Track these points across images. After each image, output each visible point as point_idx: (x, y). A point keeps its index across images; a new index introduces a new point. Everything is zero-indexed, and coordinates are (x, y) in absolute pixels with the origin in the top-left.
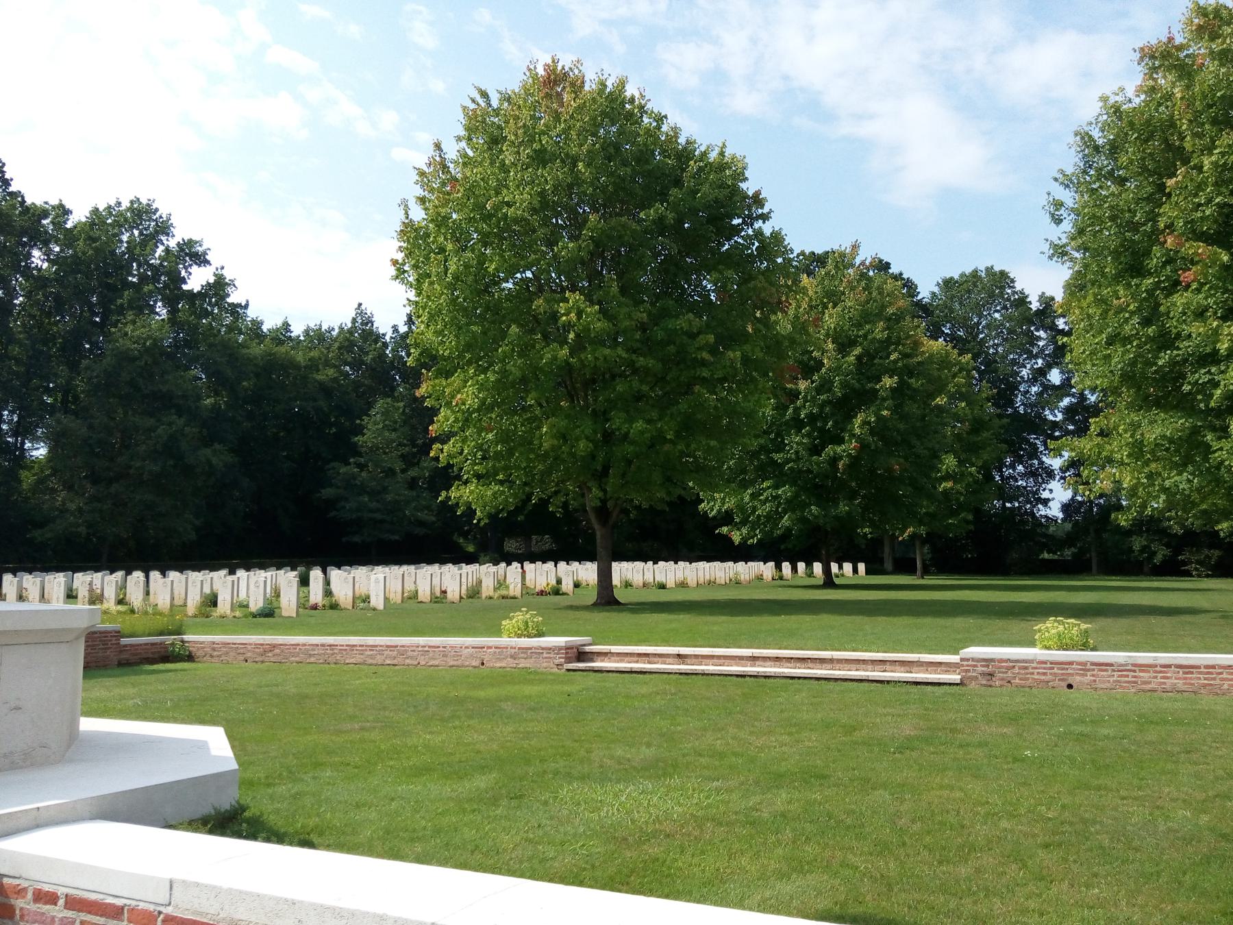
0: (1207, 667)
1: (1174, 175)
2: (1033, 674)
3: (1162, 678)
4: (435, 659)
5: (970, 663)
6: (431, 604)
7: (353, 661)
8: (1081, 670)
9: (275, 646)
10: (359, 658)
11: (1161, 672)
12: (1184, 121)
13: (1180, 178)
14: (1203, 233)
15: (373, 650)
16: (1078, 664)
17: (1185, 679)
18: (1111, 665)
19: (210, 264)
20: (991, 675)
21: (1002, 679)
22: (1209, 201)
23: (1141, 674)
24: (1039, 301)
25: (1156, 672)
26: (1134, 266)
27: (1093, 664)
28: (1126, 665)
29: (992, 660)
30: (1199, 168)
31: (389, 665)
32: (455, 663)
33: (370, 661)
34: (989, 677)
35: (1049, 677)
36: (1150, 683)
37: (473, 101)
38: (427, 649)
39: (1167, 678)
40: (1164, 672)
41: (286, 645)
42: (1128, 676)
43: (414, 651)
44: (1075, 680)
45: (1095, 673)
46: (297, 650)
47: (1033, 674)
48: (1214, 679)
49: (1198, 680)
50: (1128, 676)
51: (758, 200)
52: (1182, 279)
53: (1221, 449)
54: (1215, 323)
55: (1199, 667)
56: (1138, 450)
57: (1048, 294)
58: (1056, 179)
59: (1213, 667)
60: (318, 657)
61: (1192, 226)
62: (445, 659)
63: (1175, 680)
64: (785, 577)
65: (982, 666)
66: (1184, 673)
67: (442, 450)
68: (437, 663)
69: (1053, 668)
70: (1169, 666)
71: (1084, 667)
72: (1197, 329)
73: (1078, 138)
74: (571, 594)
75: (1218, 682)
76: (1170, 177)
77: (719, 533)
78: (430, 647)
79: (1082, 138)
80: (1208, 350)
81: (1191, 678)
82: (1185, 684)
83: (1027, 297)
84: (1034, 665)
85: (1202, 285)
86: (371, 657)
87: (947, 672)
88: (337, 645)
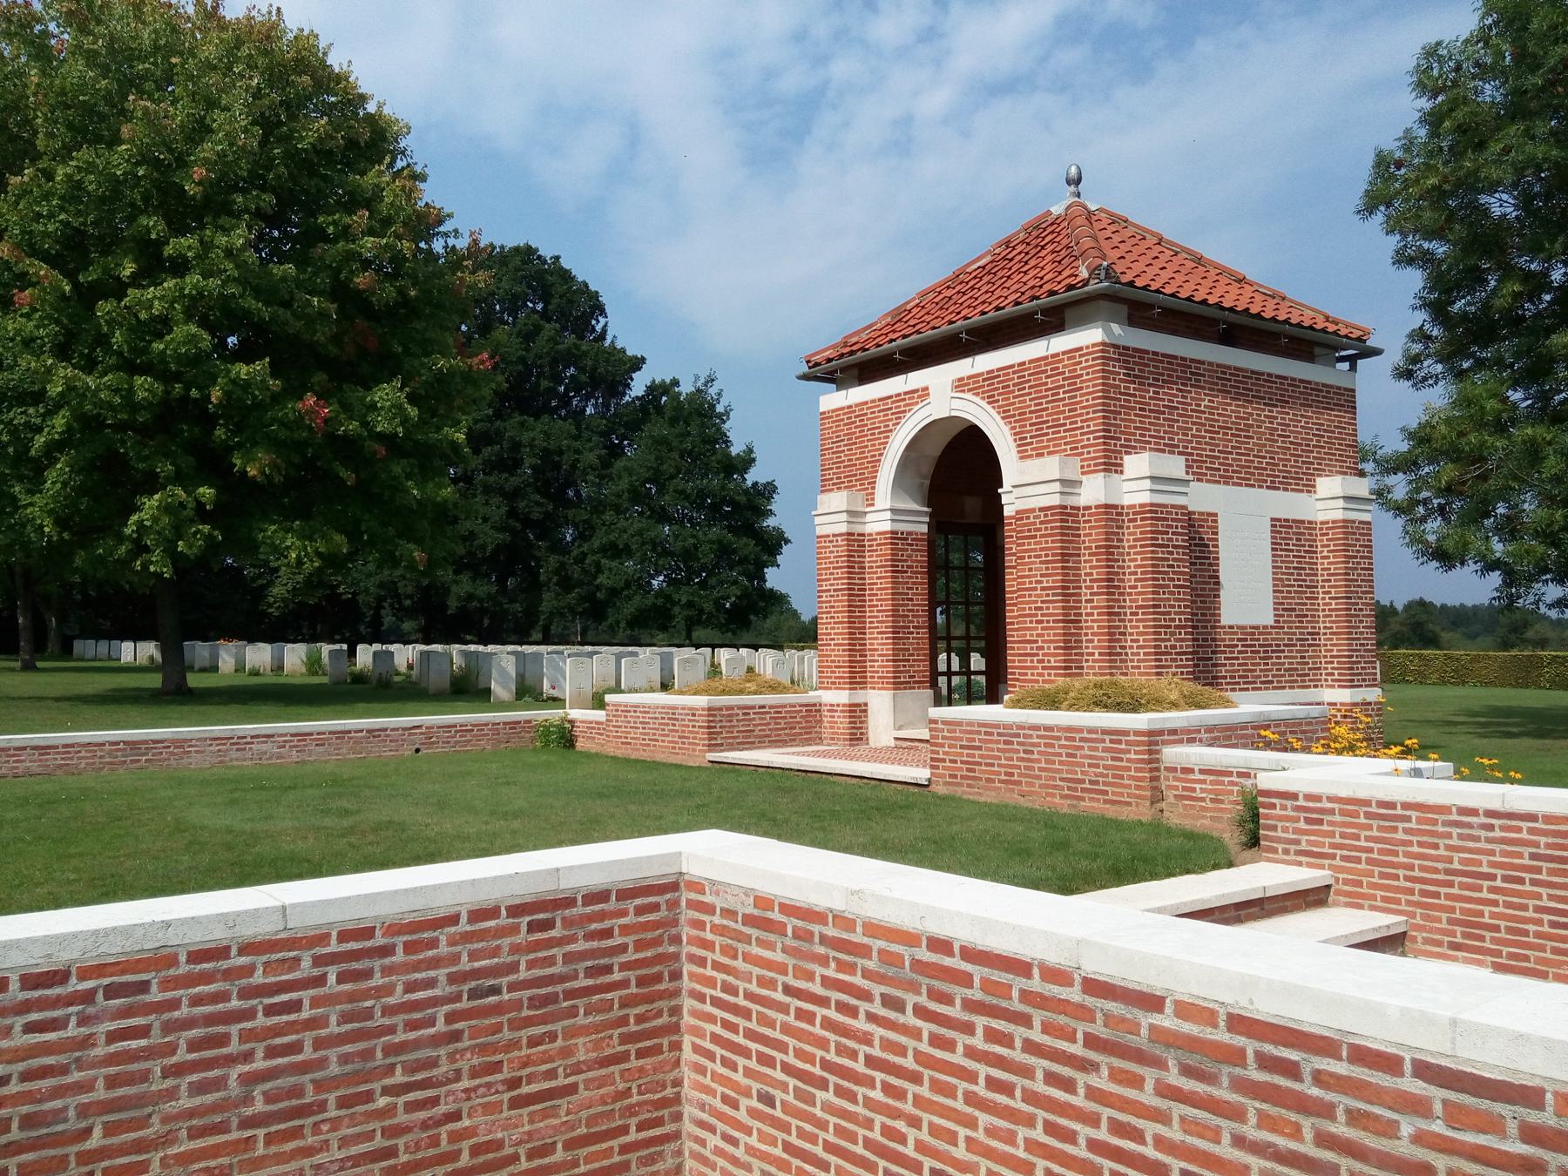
1: (20, 173)
3: (14, 762)
11: (14, 755)
12: (39, 114)
13: (26, 179)
17: (41, 760)
19: (1403, 430)
22: (51, 216)
30: (49, 175)
39: (21, 761)
48: (72, 759)
49: (54, 760)
52: (16, 299)
53: (31, 504)
54: (50, 362)
59: (72, 746)
61: (30, 239)
63: (30, 763)
66: (40, 754)
70: (25, 748)
72: (27, 362)
75: (75, 761)
76: (16, 175)
80: (36, 388)
81: (46, 760)
85: (35, 310)
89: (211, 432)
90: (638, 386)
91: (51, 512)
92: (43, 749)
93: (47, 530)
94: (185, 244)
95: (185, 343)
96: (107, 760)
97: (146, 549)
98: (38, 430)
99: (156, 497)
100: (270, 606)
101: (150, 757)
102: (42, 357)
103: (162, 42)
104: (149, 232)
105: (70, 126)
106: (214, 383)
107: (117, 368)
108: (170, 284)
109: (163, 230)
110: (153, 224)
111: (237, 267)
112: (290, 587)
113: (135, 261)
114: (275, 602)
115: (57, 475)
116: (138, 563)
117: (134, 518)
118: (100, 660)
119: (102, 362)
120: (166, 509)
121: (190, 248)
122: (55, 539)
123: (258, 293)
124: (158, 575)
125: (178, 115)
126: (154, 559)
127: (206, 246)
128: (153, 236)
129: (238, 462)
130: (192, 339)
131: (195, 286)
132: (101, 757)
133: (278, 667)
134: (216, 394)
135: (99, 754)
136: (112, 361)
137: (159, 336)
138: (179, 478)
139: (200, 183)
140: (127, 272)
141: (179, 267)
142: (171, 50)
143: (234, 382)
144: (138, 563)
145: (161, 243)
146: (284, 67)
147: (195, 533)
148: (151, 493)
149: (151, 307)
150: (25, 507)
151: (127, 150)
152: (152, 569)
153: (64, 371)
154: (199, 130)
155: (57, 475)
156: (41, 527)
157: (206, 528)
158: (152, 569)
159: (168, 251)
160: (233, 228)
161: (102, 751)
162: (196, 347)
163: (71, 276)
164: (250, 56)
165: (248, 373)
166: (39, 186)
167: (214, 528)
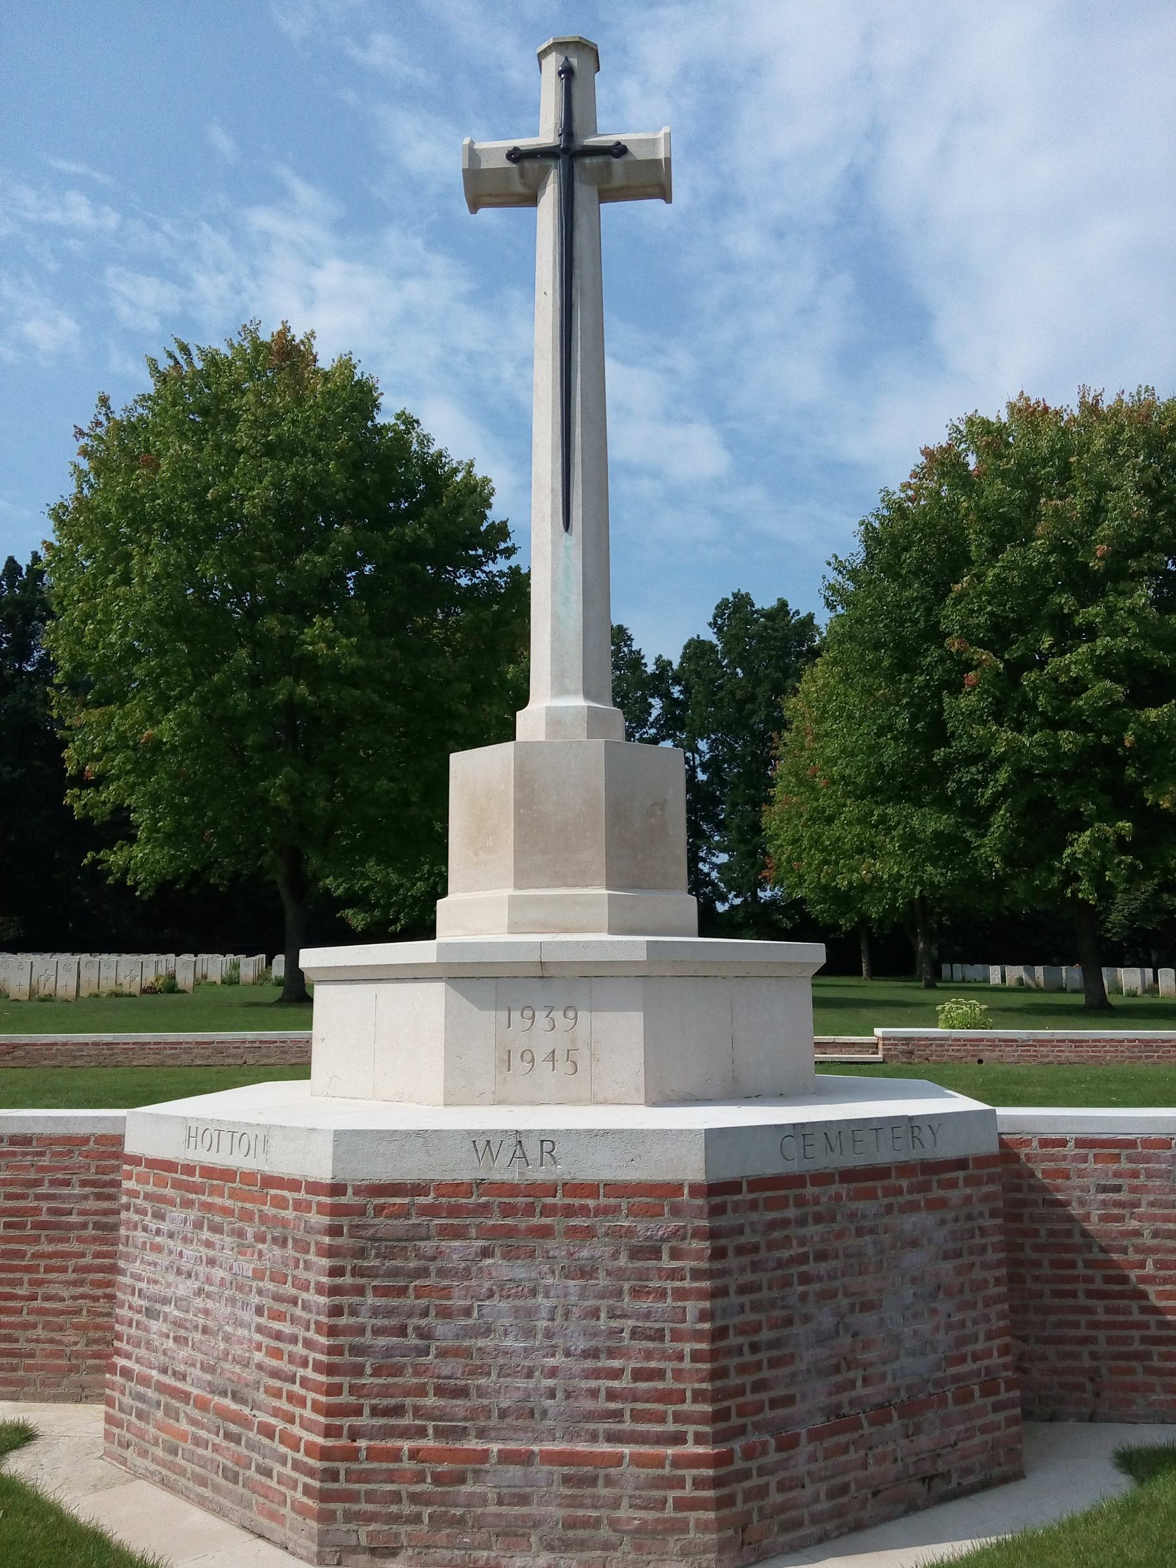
0: (1094, 1041)
2: (948, 1050)
4: (269, 1057)
5: (892, 1042)
6: (30, 1003)
7: (142, 1062)
8: (990, 1046)
9: (15, 1047)
10: (152, 1060)
11: (1056, 1046)
14: (978, 639)
15: (176, 1049)
16: (988, 1040)
17: (1077, 1052)
18: (1016, 1041)
20: (911, 1053)
21: (921, 1057)
22: (980, 609)
23: (1041, 1049)
24: (656, 664)
25: (1052, 1046)
26: (906, 661)
27: (1000, 1040)
28: (1029, 1041)
29: (911, 1039)
31: (200, 1066)
32: (298, 1060)
33: (171, 1062)
34: (909, 1055)
35: (962, 1054)
36: (1048, 1056)
37: (171, 355)
38: (257, 1045)
39: (1063, 1051)
40: (1059, 1046)
41: (35, 1045)
42: (1030, 1051)
43: (239, 1048)
44: (985, 1056)
45: (1002, 1048)
46: (54, 1051)
47: (948, 1050)
48: (1100, 1051)
49: (1086, 1052)
50: (1030, 1051)
51: (501, 531)
55: (1087, 1041)
56: (910, 839)
57: (665, 658)
58: (829, 564)
60: (88, 1059)
61: (968, 631)
62: (284, 1056)
63: (1068, 1054)
64: (181, 985)
65: (902, 1044)
66: (1076, 1047)
67: (79, 797)
68: (272, 1062)
69: (966, 1045)
70: (1064, 1041)
71: (993, 1043)
72: (978, 731)
73: (863, 527)
74: (191, 992)
77: (341, 916)
78: (261, 1042)
79: (867, 528)
82: (1076, 1056)
83: (643, 658)
84: (949, 1043)
86: (173, 1057)
87: (860, 1052)
88: (119, 1044)
89: (1123, 771)
90: (709, 635)
91: (998, 851)
92: (1078, 1042)
93: (997, 866)
94: (1094, 612)
95: (1100, 698)
96: (1127, 1054)
97: (1077, 879)
98: (984, 784)
99: (1088, 833)
100: (1108, 931)
101: (1160, 1054)
102: (988, 725)
103: (1058, 447)
104: (1062, 608)
105: (992, 535)
106: (1126, 729)
107: (1041, 727)
108: (1084, 648)
109: (1074, 605)
110: (1065, 601)
111: (1139, 624)
112: (1126, 912)
113: (1051, 634)
114: (1113, 928)
115: (1000, 818)
116: (1069, 891)
117: (1068, 851)
118: (969, 982)
119: (1028, 723)
120: (1097, 842)
121: (1097, 615)
122: (1001, 873)
123: (1157, 643)
124: (1085, 902)
125: (1077, 504)
126: (1082, 887)
127: (1111, 611)
128: (1066, 611)
129: (1150, 797)
130: (1107, 693)
131: (1105, 647)
132: (1122, 1052)
133: (1153, 989)
134: (1129, 739)
135: (1120, 1049)
136: (1037, 720)
137: (1078, 694)
138: (1101, 816)
139: (1102, 558)
140: (1046, 645)
141: (1090, 632)
142: (1066, 452)
143: (1143, 725)
144: (1069, 891)
145: (1070, 616)
146: (1160, 437)
147: (1119, 864)
148: (1082, 830)
149: (1069, 670)
150: (977, 848)
151: (1041, 544)
152: (1080, 896)
153: (1007, 735)
154: (1096, 512)
155: (1000, 818)
156: (992, 864)
157: (1129, 859)
158: (1080, 896)
159: (1078, 620)
160: (1133, 590)
161: (1122, 1046)
162: (1111, 699)
163: (998, 654)
164: (1131, 437)
165: (1158, 716)
166: (975, 588)
167: (1136, 858)
